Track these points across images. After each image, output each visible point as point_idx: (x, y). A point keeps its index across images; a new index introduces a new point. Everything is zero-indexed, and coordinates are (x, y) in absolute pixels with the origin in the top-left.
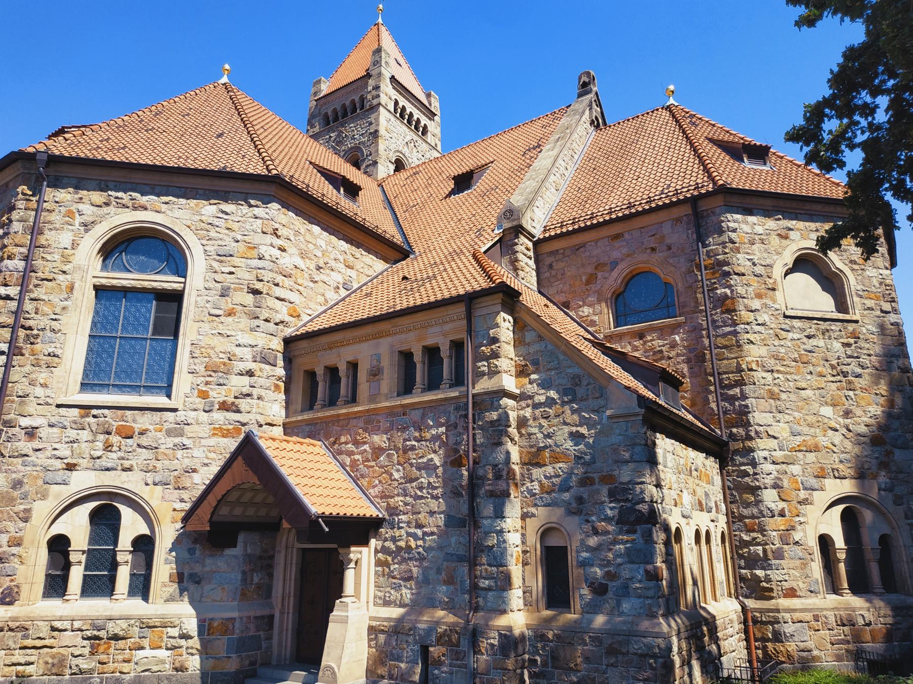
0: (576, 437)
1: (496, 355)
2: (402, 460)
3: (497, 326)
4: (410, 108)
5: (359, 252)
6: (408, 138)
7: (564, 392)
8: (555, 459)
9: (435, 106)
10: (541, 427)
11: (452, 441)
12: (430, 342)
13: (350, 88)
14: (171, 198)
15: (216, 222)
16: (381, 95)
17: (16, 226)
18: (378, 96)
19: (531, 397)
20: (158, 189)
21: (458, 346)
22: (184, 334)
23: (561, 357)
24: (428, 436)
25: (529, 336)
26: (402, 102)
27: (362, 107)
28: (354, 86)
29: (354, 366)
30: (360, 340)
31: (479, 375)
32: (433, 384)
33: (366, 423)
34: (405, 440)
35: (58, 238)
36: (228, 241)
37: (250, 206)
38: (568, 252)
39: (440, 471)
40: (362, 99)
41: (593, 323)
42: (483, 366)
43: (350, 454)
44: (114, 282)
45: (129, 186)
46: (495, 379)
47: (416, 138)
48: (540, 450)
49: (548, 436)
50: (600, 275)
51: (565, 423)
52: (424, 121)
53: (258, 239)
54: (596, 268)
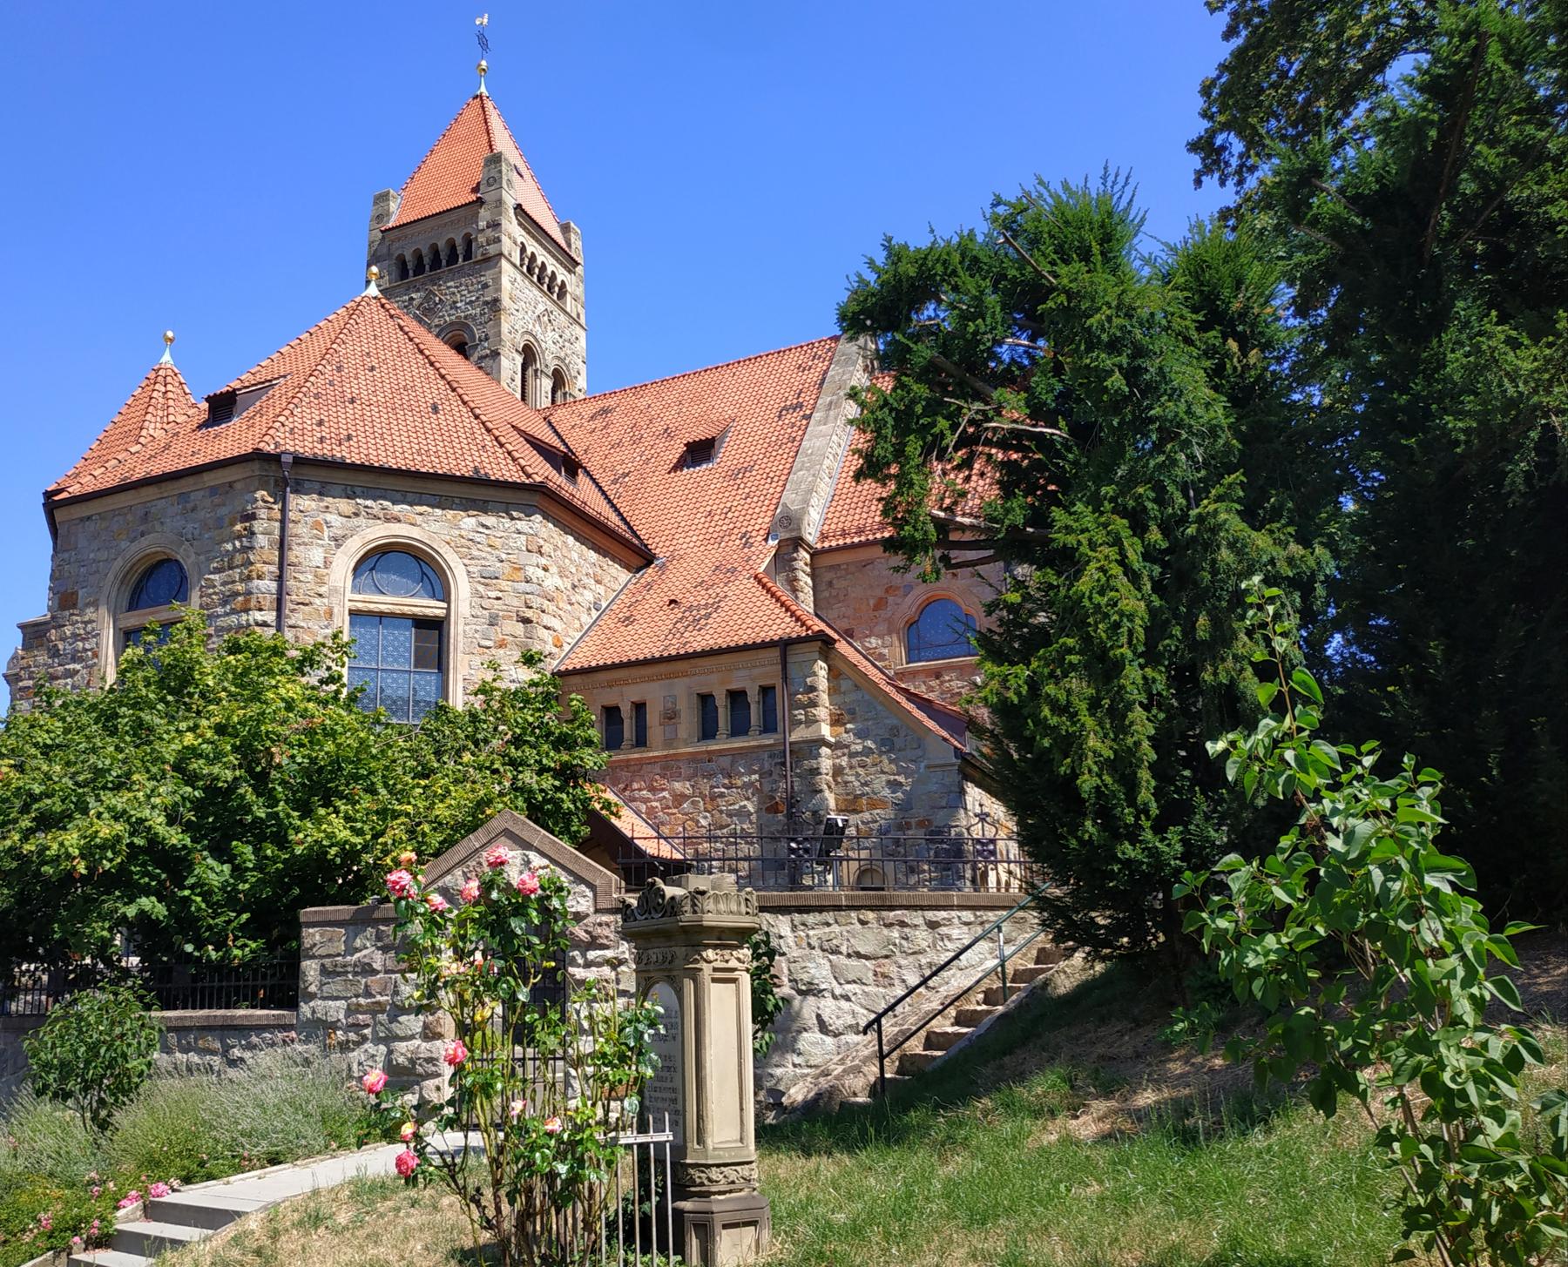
0: (894, 785)
1: (814, 704)
2: (710, 807)
3: (815, 674)
4: (542, 257)
5: (607, 563)
6: (541, 308)
7: (882, 742)
8: (873, 805)
9: (577, 248)
10: (858, 775)
11: (767, 788)
12: (734, 686)
13: (446, 219)
14: (425, 508)
15: (478, 537)
16: (504, 239)
17: (261, 540)
18: (498, 240)
19: (847, 747)
20: (410, 497)
21: (767, 691)
22: (455, 668)
23: (880, 708)
24: (739, 783)
25: (845, 685)
26: (533, 247)
27: (468, 256)
28: (454, 216)
29: (640, 708)
30: (651, 680)
31: (796, 723)
32: (739, 729)
33: (663, 768)
34: (712, 787)
35: (309, 554)
36: (492, 561)
37: (513, 519)
38: (852, 568)
39: (754, 818)
40: (469, 242)
41: (881, 657)
42: (800, 714)
43: (645, 801)
44: (372, 607)
45: (378, 493)
46: (814, 726)
47: (551, 306)
48: (857, 797)
49: (866, 784)
50: (890, 599)
51: (883, 772)
52: (562, 274)
53: (525, 558)
54: (887, 591)
